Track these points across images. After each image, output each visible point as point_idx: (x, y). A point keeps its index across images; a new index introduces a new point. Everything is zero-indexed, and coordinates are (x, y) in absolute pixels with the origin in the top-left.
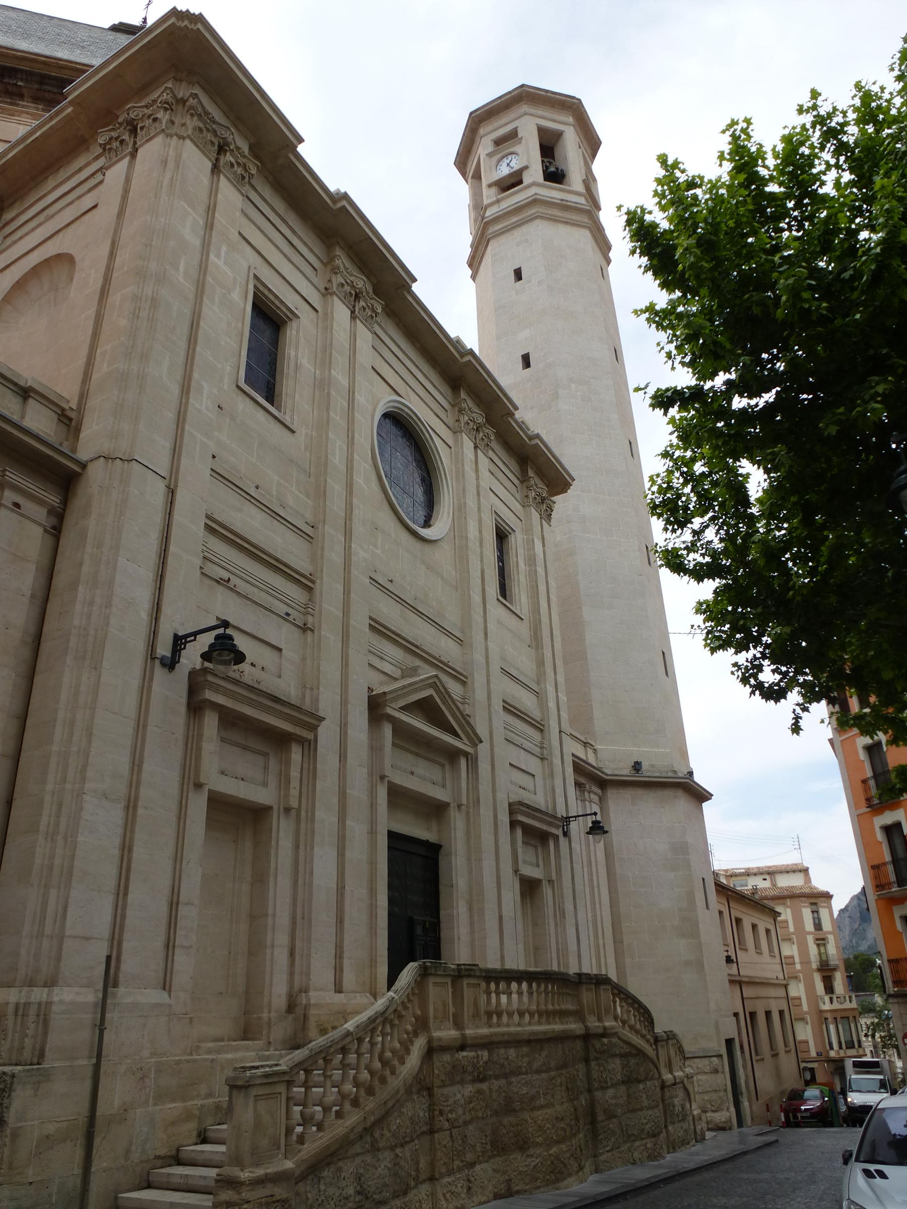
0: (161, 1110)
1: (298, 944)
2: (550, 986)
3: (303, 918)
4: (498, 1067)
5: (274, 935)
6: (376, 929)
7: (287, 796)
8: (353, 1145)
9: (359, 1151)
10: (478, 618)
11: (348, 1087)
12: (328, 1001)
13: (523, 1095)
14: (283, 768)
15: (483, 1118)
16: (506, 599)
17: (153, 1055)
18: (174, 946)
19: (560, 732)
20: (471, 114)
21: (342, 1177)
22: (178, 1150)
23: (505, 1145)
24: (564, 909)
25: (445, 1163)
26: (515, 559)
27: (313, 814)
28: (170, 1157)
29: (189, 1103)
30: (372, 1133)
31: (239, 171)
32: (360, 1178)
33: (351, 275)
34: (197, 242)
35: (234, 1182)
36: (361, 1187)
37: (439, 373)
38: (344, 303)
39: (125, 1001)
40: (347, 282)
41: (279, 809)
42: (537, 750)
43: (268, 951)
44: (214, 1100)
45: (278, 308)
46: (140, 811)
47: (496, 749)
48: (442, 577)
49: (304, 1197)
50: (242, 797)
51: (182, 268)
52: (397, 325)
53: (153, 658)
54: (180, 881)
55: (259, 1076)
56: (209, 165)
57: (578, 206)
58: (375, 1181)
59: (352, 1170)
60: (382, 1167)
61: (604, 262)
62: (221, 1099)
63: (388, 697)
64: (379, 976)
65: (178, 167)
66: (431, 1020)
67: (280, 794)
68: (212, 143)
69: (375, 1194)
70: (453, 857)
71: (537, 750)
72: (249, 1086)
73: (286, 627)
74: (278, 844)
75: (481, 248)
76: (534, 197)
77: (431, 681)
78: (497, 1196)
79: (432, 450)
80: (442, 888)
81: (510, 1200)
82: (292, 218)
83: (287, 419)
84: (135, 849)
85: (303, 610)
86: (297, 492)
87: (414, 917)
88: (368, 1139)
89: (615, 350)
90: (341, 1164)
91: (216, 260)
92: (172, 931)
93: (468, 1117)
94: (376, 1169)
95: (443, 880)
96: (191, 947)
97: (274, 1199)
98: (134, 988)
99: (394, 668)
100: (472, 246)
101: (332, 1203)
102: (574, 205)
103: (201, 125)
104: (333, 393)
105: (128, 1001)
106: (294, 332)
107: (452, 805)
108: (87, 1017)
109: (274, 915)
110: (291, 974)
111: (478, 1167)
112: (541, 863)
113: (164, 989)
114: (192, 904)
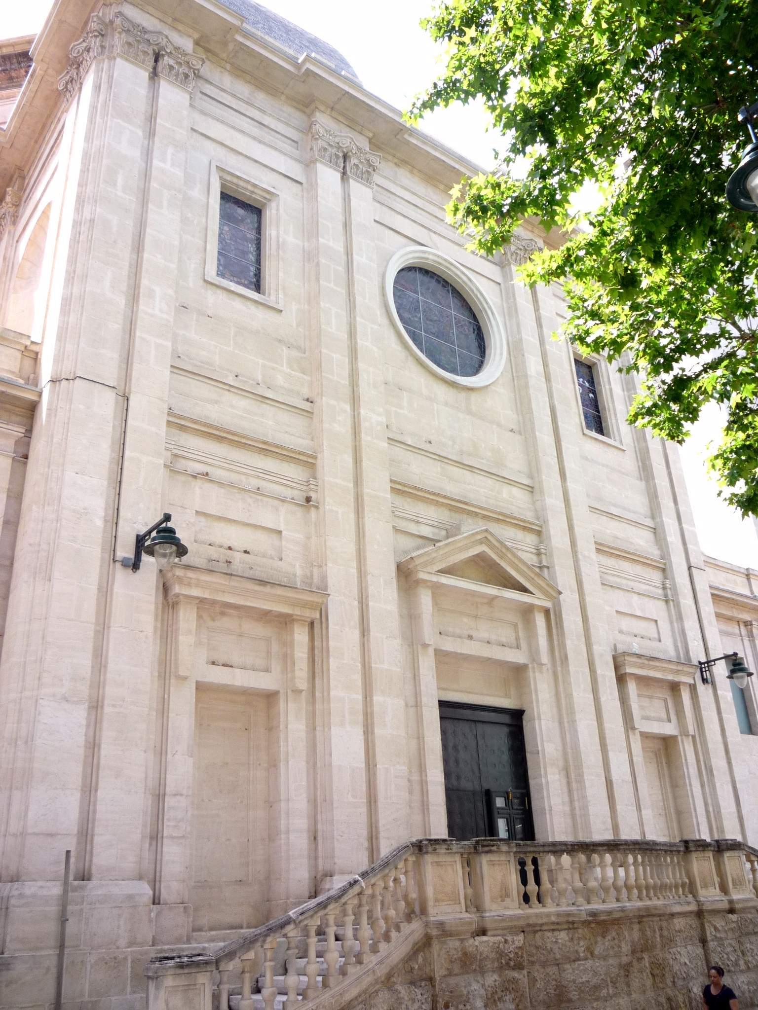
2: (639, 857)
6: (428, 805)
10: (549, 459)
13: (583, 983)
14: (521, 634)
17: (131, 944)
19: (690, 568)
24: (711, 767)
26: (607, 387)
31: (183, 69)
34: (136, 154)
40: (330, 145)
45: (253, 192)
46: (107, 710)
47: (588, 599)
51: (120, 182)
52: (411, 172)
53: (114, 561)
56: (145, 75)
63: (417, 562)
65: (111, 87)
68: (145, 53)
70: (537, 722)
77: (479, 537)
80: (528, 756)
82: (261, 98)
85: (305, 488)
91: (162, 165)
95: (529, 748)
99: (436, 530)
103: (131, 40)
104: (323, 261)
106: (274, 212)
107: (530, 666)
108: (53, 909)
112: (673, 717)
114: (182, 795)
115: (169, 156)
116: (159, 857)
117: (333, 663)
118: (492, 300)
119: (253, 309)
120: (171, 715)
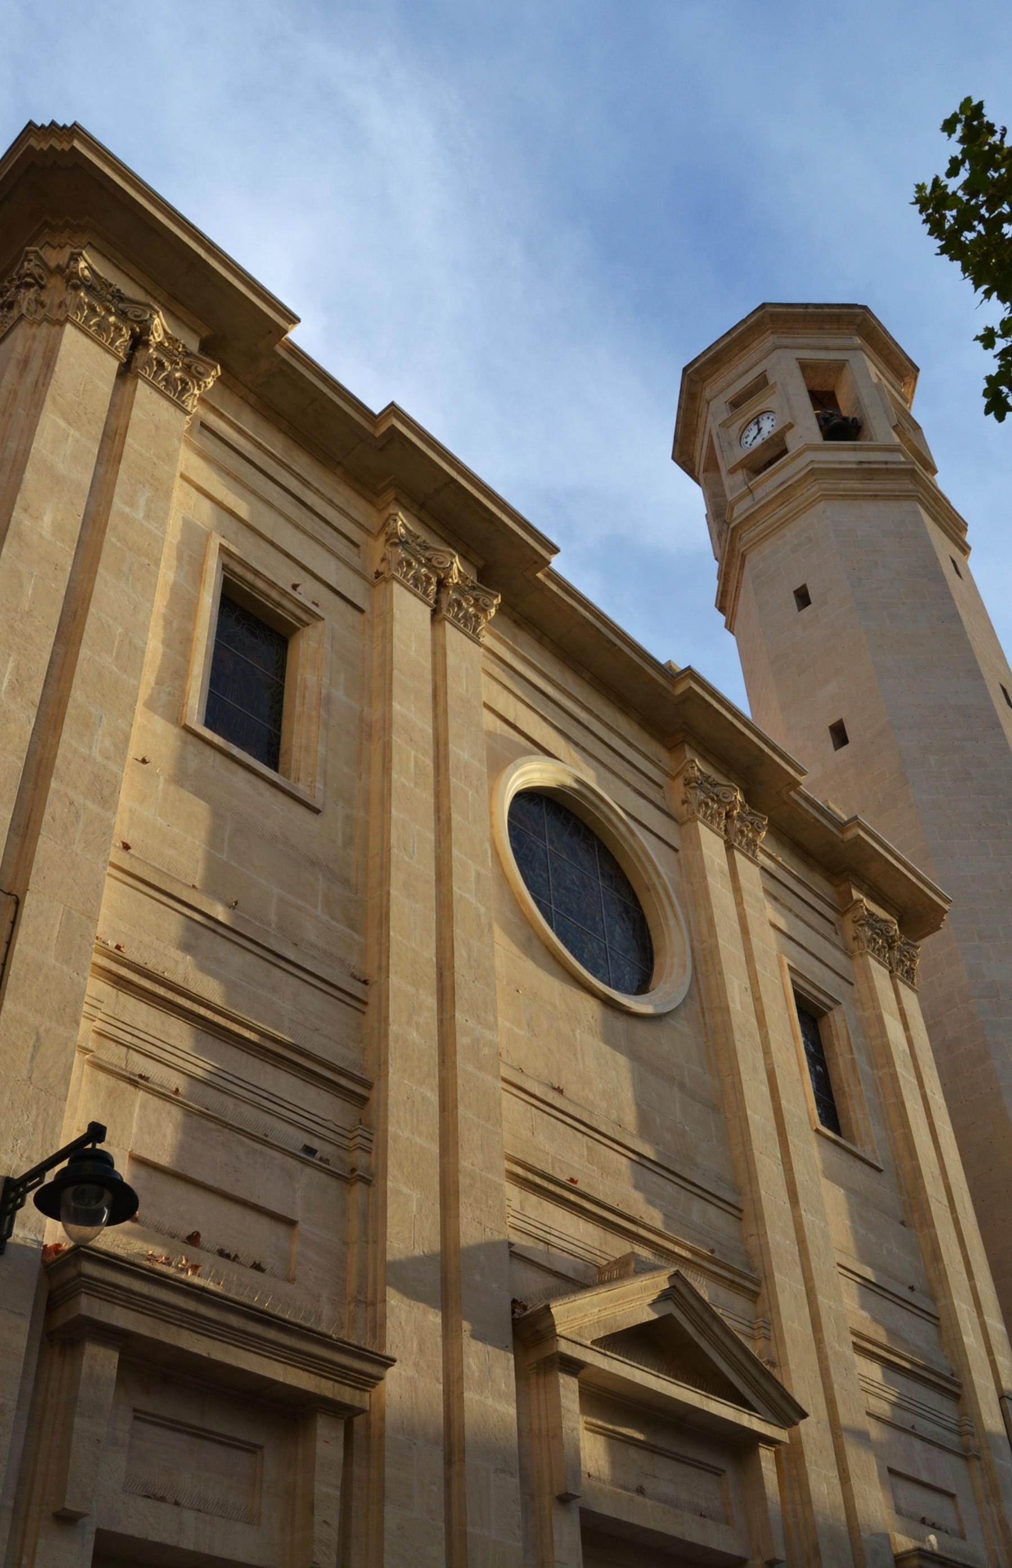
16: (840, 1135)
20: (685, 370)
33: (427, 548)
37: (639, 724)
38: (415, 595)
42: (952, 1440)
45: (279, 604)
48: (682, 1086)
50: (191, 1548)
52: (540, 641)
56: (113, 365)
57: (889, 466)
61: (956, 553)
71: (952, 1440)
73: (306, 1177)
75: (734, 573)
76: (810, 468)
79: (638, 857)
82: (301, 463)
83: (302, 790)
86: (326, 918)
89: (1004, 691)
100: (719, 577)
102: (884, 466)
112: (369, 1389)
115: (142, 501)
117: (392, 1517)
118: (666, 874)
119: (268, 794)
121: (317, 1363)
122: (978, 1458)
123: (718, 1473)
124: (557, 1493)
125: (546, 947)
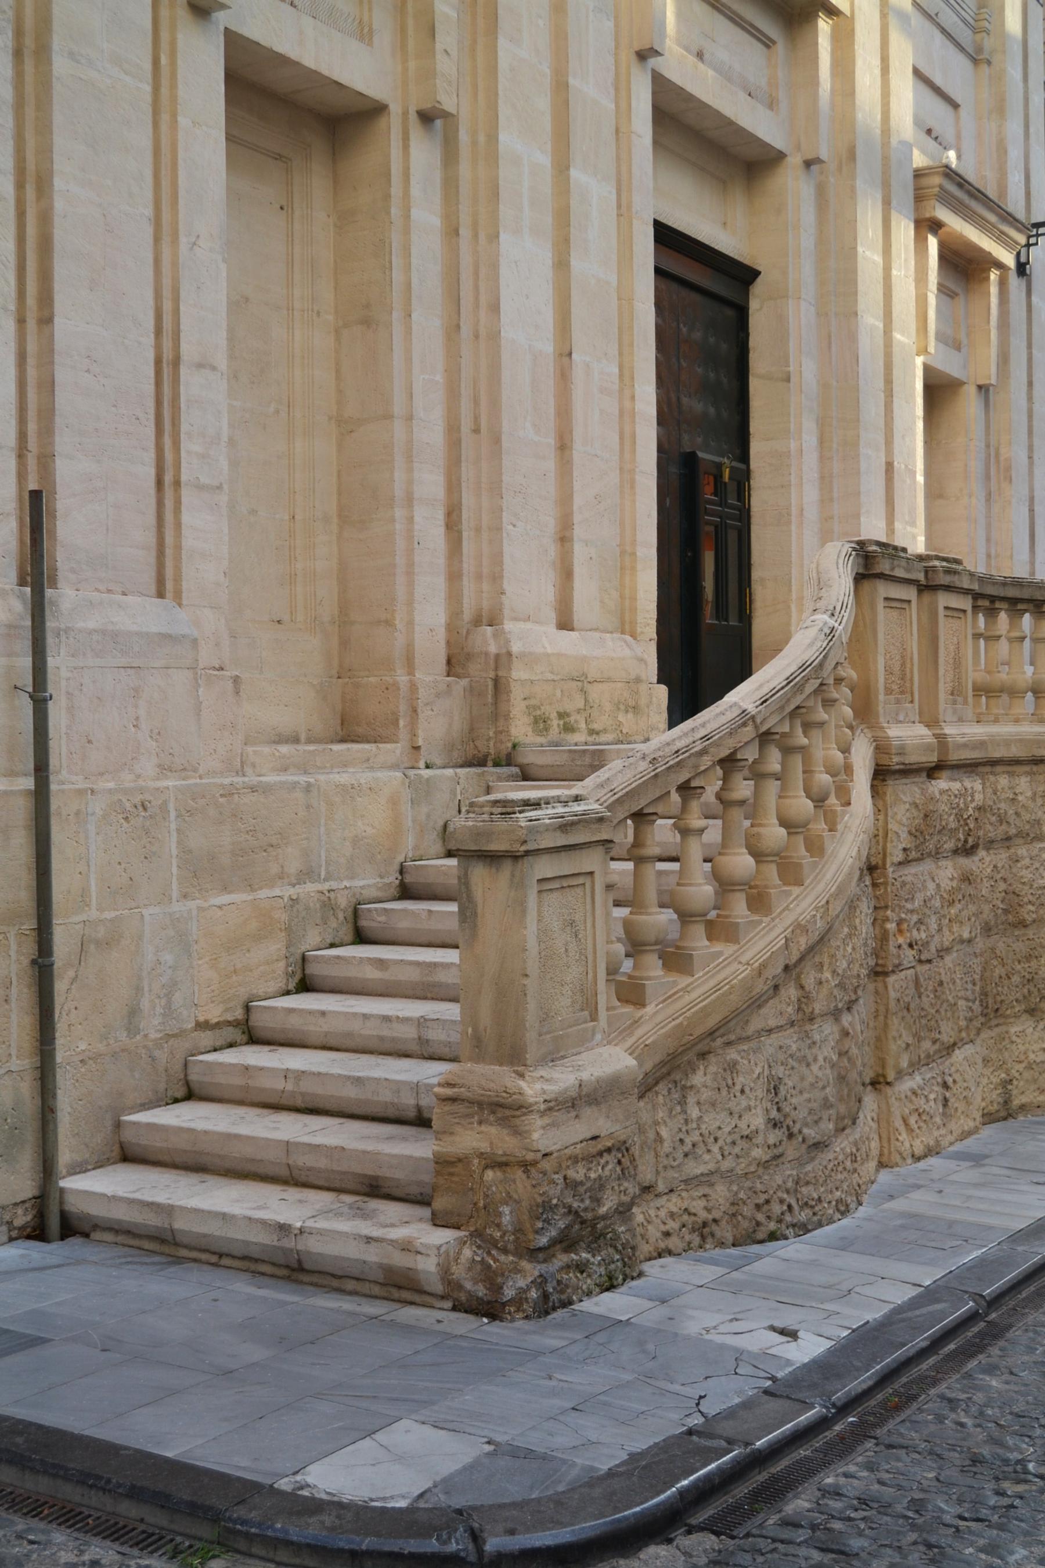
0: (200, 909)
1: (468, 500)
3: (477, 431)
4: (994, 819)
5: (410, 470)
7: (429, 74)
8: (759, 1007)
9: (772, 1023)
11: (741, 863)
12: (549, 651)
15: (969, 941)
18: (177, 483)
21: (738, 1087)
22: (247, 1009)
23: (1002, 1001)
25: (908, 1045)
27: (493, 138)
28: (229, 1023)
29: (263, 894)
30: (798, 977)
32: (776, 1088)
35: (501, 1106)
36: (779, 1110)
39: (81, 625)
41: (405, 113)
42: (964, 35)
43: (399, 513)
44: (319, 887)
49: (651, 1135)
54: (176, 300)
55: (548, 828)
58: (806, 1096)
59: (758, 1070)
60: (820, 1058)
62: (334, 885)
64: (641, 594)
66: (881, 697)
67: (405, 70)
69: (806, 1125)
71: (964, 35)
72: (527, 853)
74: (407, 216)
78: (989, 1118)
81: (1011, 1122)
84: (58, 183)
87: (700, 454)
88: (791, 992)
90: (732, 1054)
92: (167, 441)
93: (947, 938)
94: (808, 1065)
95: (759, 363)
96: (220, 487)
97: (600, 1146)
98: (97, 590)
101: (715, 1149)
105: (91, 625)
109: (410, 418)
110: (454, 577)
111: (958, 1055)
113: (161, 594)
114: (214, 368)
116: (169, 540)
120: (183, 121)
121: (666, 1025)
122: (989, 63)
123: (768, 43)
124: (637, 47)
125: (387, 1138)
